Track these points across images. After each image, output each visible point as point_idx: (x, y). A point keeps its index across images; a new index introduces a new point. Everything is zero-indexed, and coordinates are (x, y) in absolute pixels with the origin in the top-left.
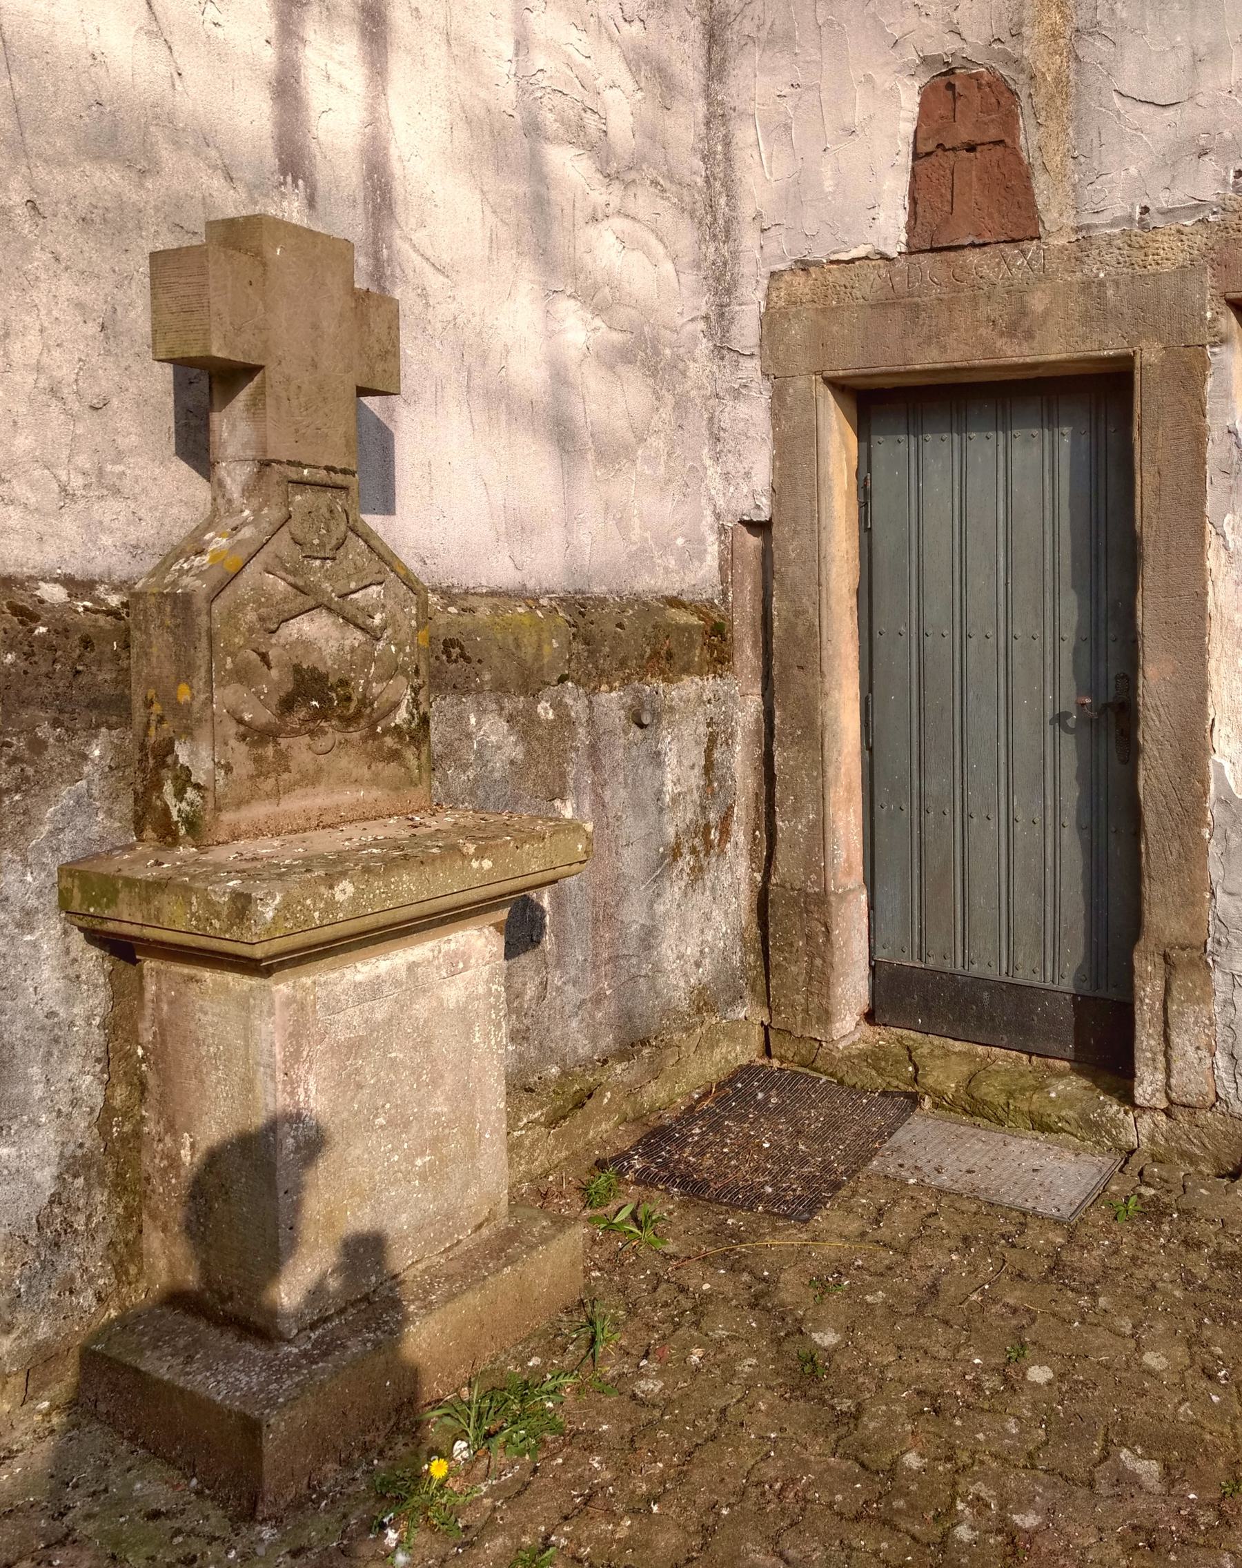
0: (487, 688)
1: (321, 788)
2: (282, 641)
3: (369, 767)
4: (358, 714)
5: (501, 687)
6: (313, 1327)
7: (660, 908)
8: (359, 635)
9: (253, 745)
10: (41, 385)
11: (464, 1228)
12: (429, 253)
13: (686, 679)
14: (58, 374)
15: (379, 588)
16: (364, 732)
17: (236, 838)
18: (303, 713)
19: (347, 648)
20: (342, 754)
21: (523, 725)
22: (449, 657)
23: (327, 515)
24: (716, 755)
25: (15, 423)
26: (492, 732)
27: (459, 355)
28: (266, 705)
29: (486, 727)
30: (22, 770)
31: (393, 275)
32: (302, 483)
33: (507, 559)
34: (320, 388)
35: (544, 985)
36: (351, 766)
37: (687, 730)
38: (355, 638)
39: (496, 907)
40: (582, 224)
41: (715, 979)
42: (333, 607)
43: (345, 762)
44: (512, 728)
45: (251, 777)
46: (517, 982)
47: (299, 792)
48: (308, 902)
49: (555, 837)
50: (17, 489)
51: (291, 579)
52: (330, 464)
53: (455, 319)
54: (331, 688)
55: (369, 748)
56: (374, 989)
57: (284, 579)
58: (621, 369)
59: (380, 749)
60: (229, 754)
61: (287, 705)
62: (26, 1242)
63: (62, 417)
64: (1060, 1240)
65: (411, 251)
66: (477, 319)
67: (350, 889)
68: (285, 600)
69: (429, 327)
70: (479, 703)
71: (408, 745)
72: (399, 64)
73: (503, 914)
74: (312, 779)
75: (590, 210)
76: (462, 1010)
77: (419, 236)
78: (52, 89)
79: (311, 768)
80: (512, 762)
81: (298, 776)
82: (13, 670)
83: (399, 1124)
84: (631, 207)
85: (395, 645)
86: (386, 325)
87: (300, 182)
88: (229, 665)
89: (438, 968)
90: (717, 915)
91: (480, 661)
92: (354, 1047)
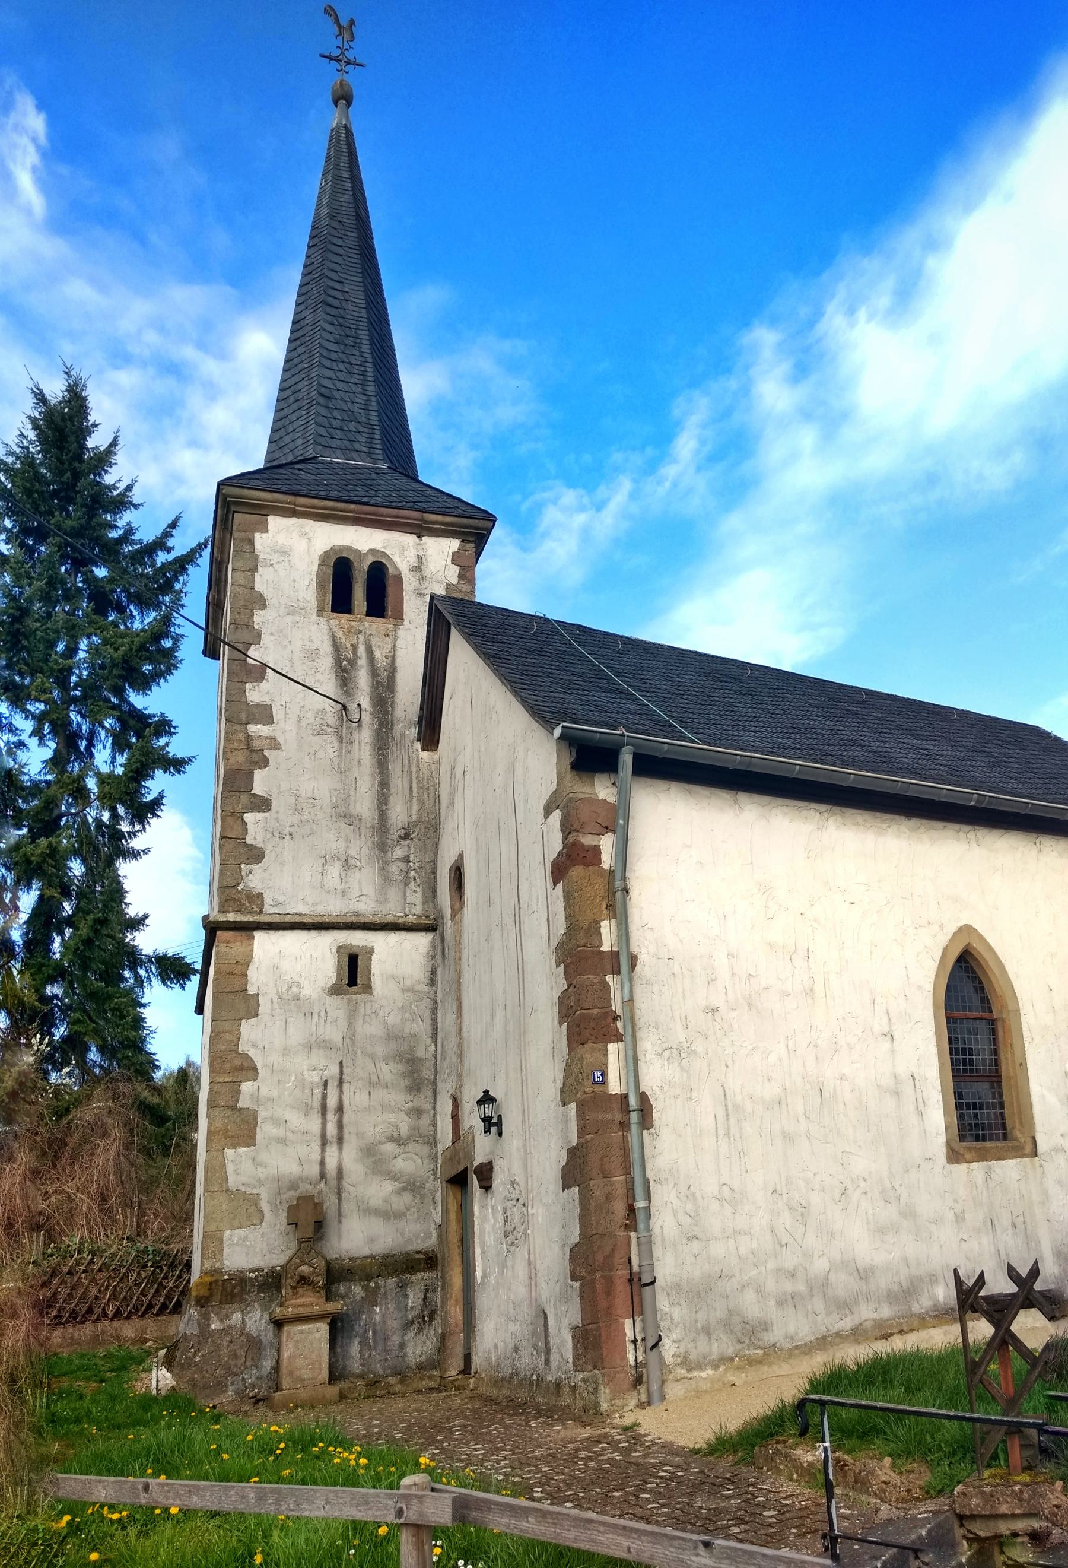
5: (360, 1279)
7: (406, 1338)
13: (418, 1274)
21: (366, 1288)
24: (428, 1295)
35: (370, 1354)
37: (417, 1288)
41: (426, 1361)
43: (309, 1293)
56: (302, 1332)
58: (403, 1193)
61: (298, 1283)
72: (345, 1146)
73: (329, 1321)
74: (302, 1296)
76: (320, 1339)
77: (349, 1181)
83: (305, 1358)
84: (407, 1149)
90: (428, 1343)
92: (297, 1341)
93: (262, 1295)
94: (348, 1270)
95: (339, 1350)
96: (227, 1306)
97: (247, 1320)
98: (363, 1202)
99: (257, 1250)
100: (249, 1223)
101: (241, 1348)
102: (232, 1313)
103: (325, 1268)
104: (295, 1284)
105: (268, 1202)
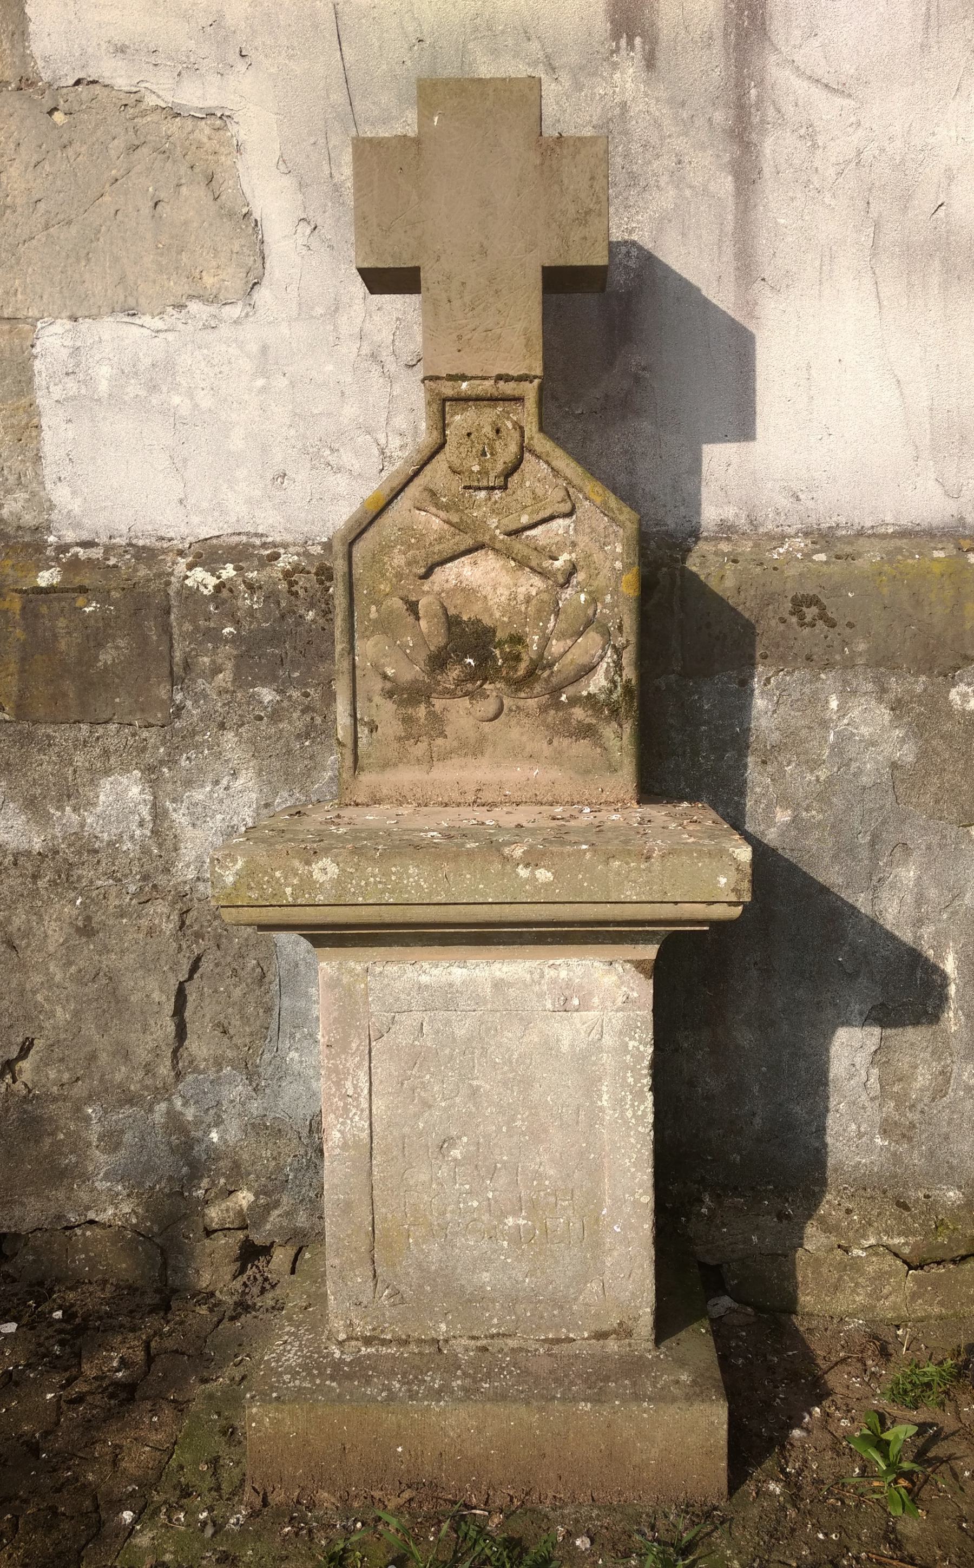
0: (860, 661)
1: (484, 761)
2: (436, 588)
3: (550, 742)
4: (531, 674)
6: (368, 1341)
8: (537, 581)
9: (401, 703)
10: (363, 352)
11: (580, 1329)
12: (820, 72)
14: (377, 338)
15: (567, 521)
16: (544, 699)
17: (377, 801)
18: (455, 672)
19: (521, 597)
20: (513, 723)
22: (802, 617)
23: (492, 435)
25: (342, 393)
26: (864, 721)
27: (861, 205)
28: (412, 661)
29: (855, 713)
30: (312, 719)
31: (763, 122)
32: (463, 400)
33: (931, 483)
34: (491, 280)
36: (524, 738)
38: (531, 585)
39: (646, 938)
42: (497, 546)
44: (899, 718)
45: (399, 739)
46: (903, 1063)
47: (456, 761)
48: (278, 874)
49: (673, 860)
50: (344, 457)
51: (443, 514)
52: (503, 372)
53: (859, 153)
54: (499, 645)
55: (550, 719)
57: (436, 516)
59: (566, 721)
60: (374, 711)
61: (438, 662)
62: (300, 1138)
63: (381, 380)
66: (898, 143)
67: (333, 870)
68: (440, 539)
69: (815, 179)
70: (846, 682)
71: (608, 720)
73: (650, 952)
78: (377, 44)
79: (472, 735)
80: (894, 766)
81: (455, 744)
82: (314, 626)
85: (589, 593)
86: (588, 175)
87: (638, 40)
88: (373, 614)
89: (541, 996)
91: (851, 625)
93: (267, 695)
94: (800, 603)
95: (745, 1038)
96: (62, 735)
97: (179, 817)
98: (905, 200)
99: (237, 442)
100: (178, 287)
101: (147, 966)
102: (95, 774)
103: (629, 586)
104: (412, 672)
105: (285, 164)
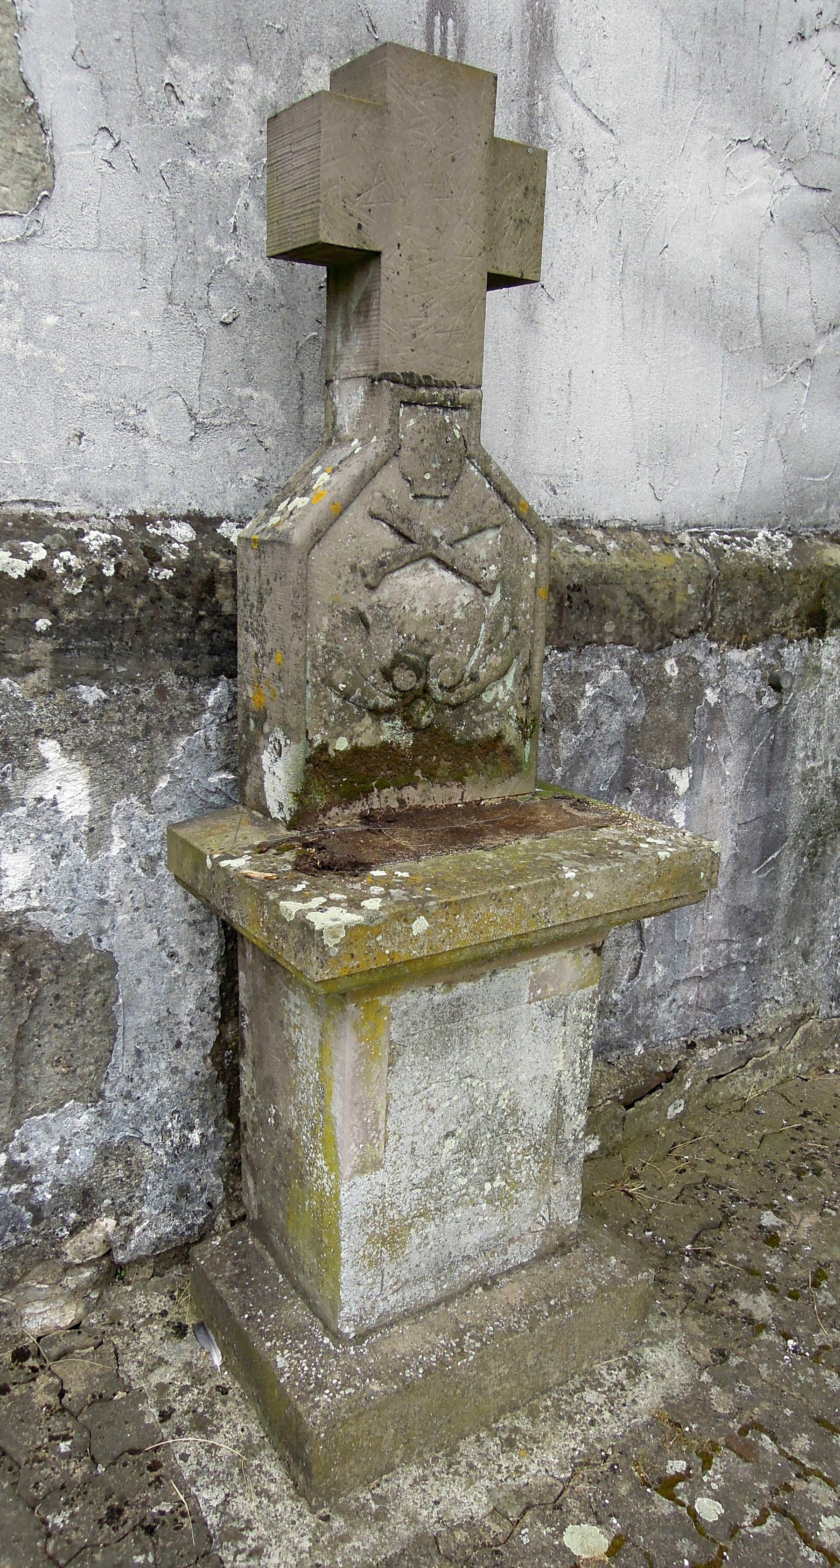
40: (784, 45)
64: (85, 1117)
65: (571, 100)
75: (796, 23)
